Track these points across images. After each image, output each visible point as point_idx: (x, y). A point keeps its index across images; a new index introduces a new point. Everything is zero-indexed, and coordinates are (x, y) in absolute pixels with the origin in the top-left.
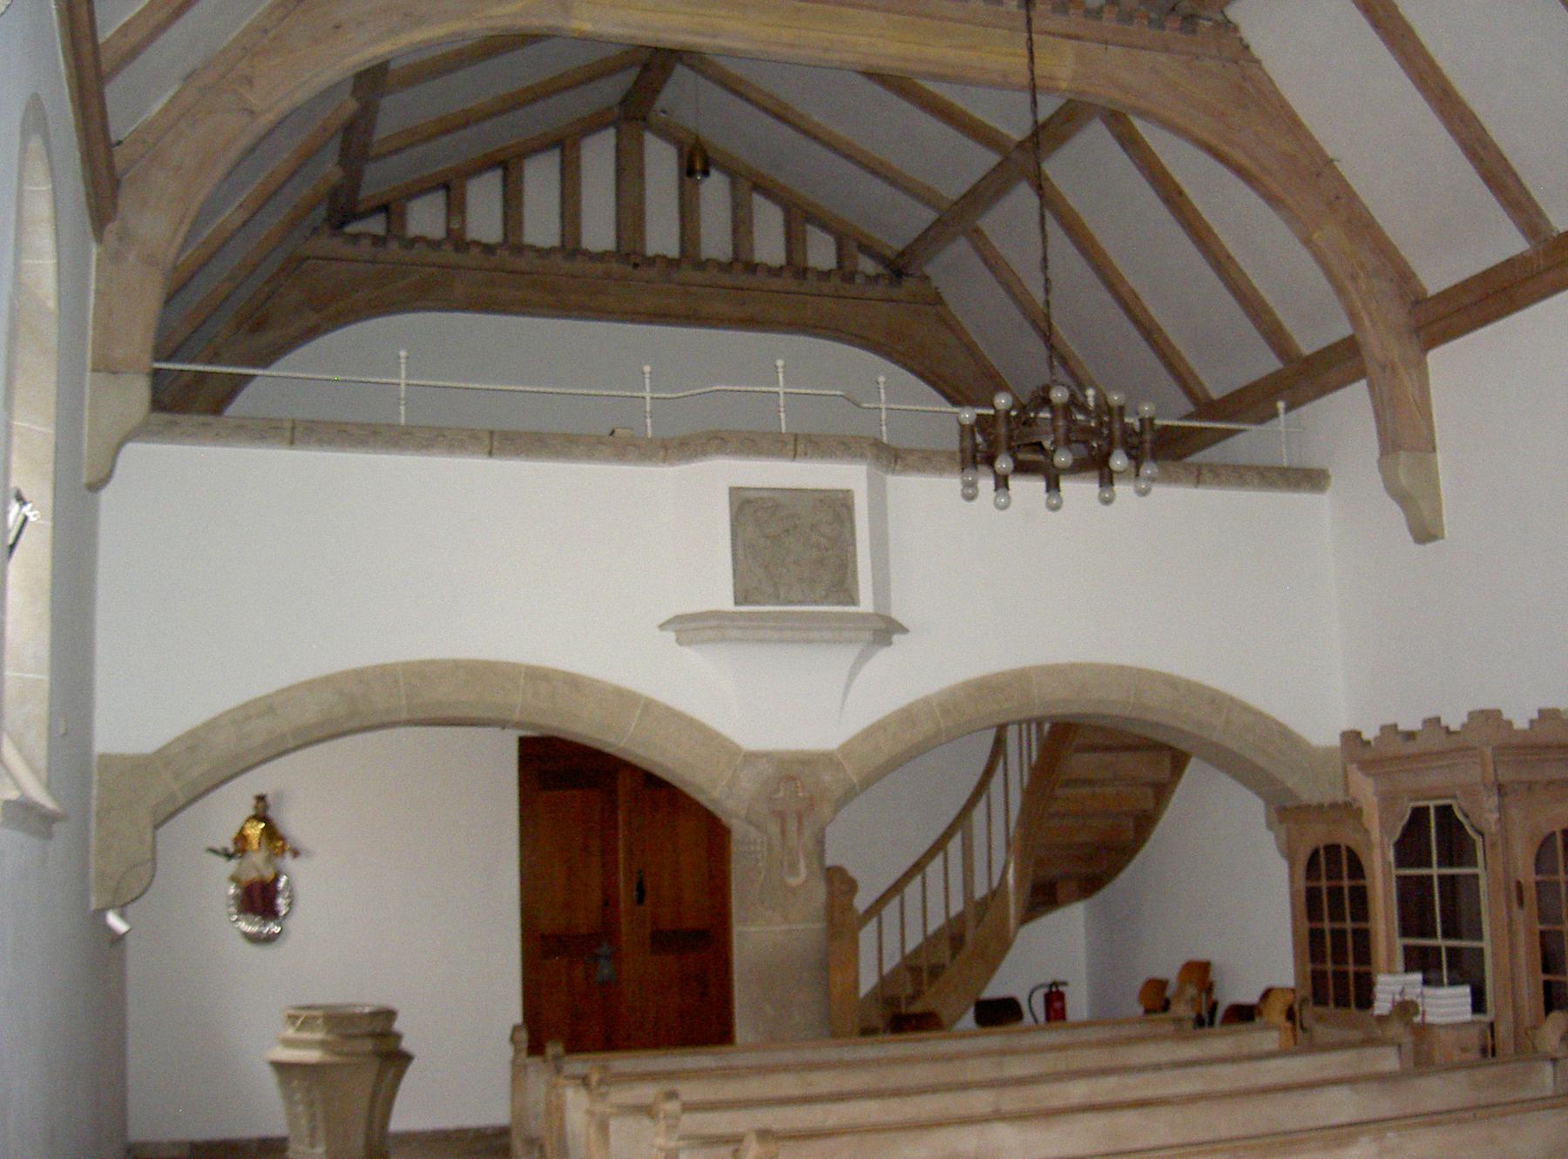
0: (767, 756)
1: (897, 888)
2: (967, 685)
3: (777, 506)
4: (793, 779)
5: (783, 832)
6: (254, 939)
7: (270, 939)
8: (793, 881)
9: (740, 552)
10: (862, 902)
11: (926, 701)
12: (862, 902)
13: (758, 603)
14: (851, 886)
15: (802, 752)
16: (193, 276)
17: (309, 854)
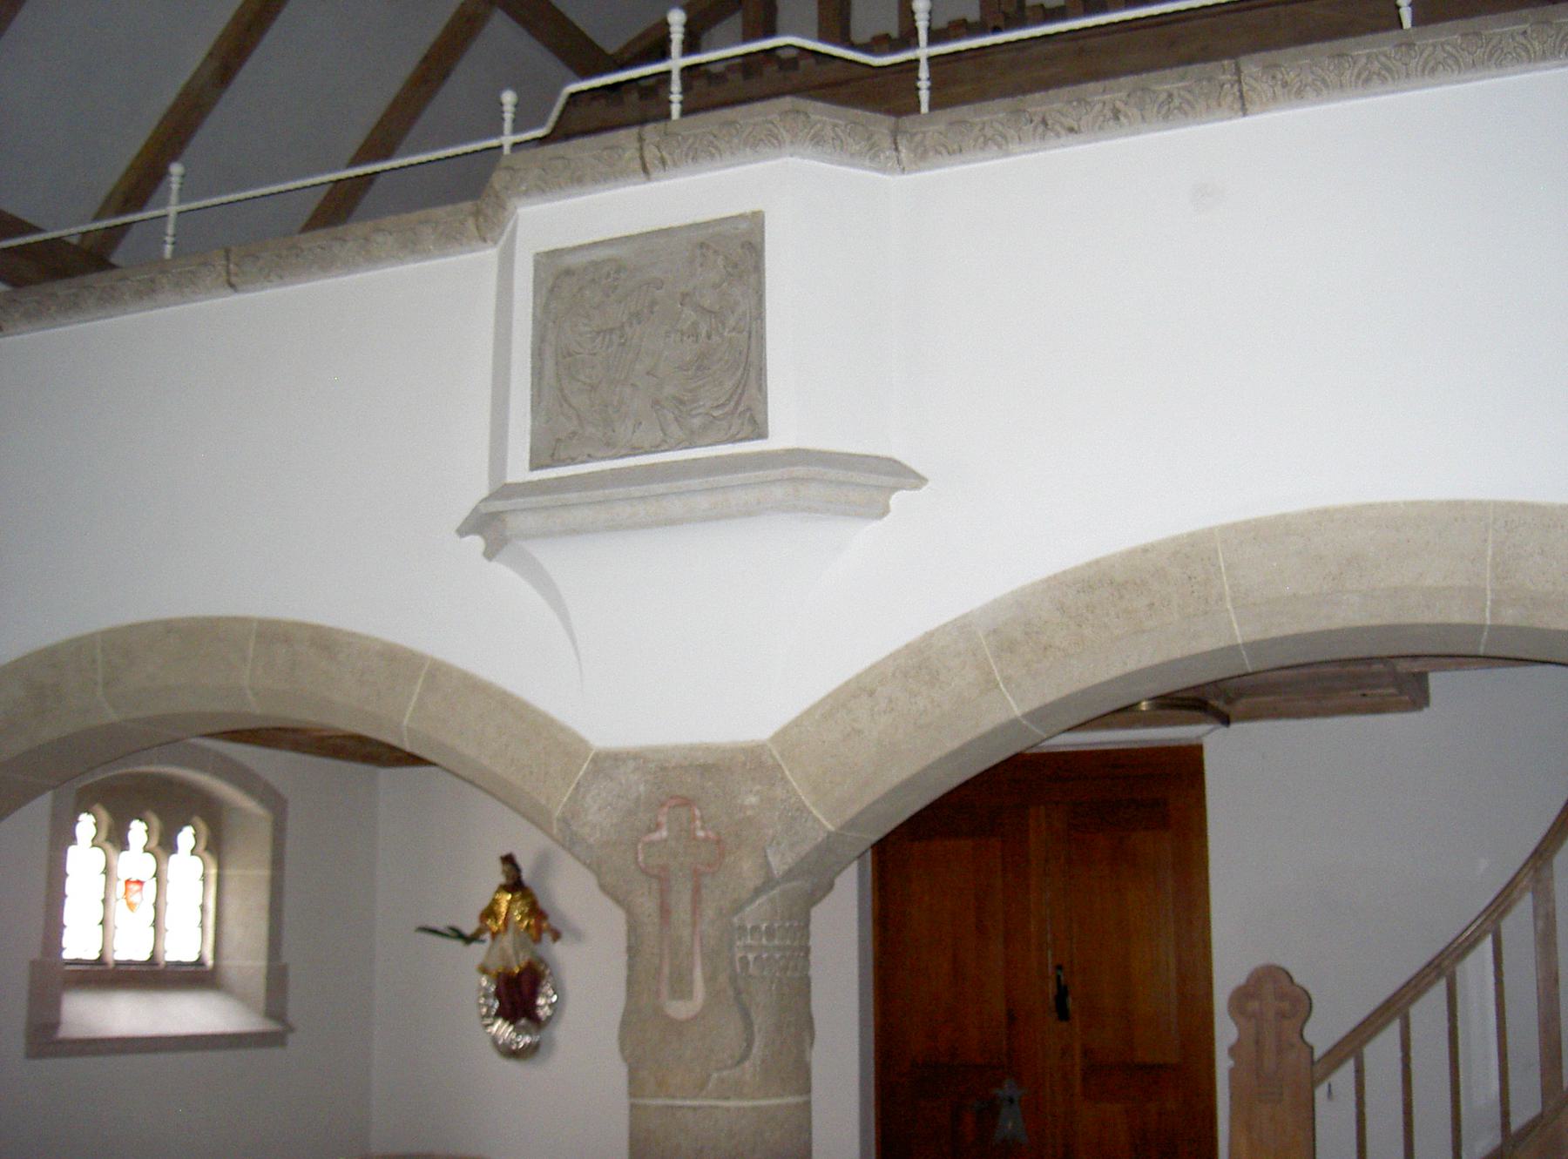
0: (638, 757)
1: (1395, 1007)
2: (1056, 583)
3: (619, 267)
4: (687, 803)
5: (665, 911)
6: (510, 1053)
7: (530, 1051)
8: (680, 1010)
9: (550, 365)
10: (1322, 1033)
11: (962, 626)
12: (1322, 1033)
13: (573, 461)
14: (1299, 1004)
15: (708, 749)
16: (822, 86)
17: (578, 936)
